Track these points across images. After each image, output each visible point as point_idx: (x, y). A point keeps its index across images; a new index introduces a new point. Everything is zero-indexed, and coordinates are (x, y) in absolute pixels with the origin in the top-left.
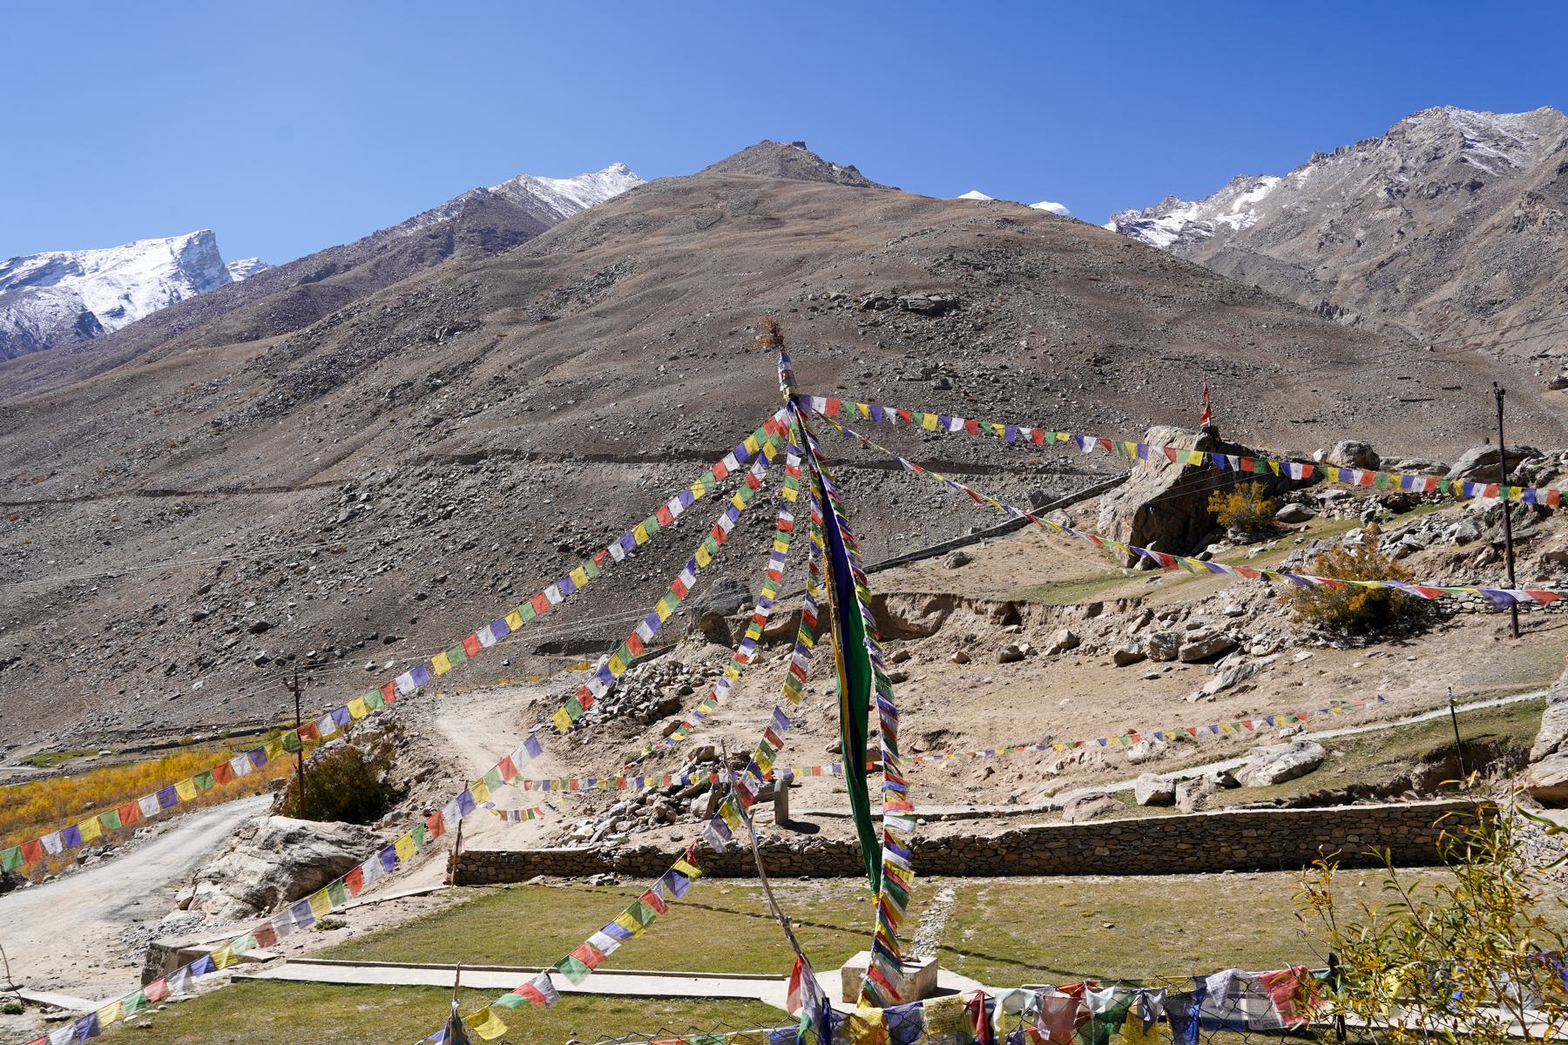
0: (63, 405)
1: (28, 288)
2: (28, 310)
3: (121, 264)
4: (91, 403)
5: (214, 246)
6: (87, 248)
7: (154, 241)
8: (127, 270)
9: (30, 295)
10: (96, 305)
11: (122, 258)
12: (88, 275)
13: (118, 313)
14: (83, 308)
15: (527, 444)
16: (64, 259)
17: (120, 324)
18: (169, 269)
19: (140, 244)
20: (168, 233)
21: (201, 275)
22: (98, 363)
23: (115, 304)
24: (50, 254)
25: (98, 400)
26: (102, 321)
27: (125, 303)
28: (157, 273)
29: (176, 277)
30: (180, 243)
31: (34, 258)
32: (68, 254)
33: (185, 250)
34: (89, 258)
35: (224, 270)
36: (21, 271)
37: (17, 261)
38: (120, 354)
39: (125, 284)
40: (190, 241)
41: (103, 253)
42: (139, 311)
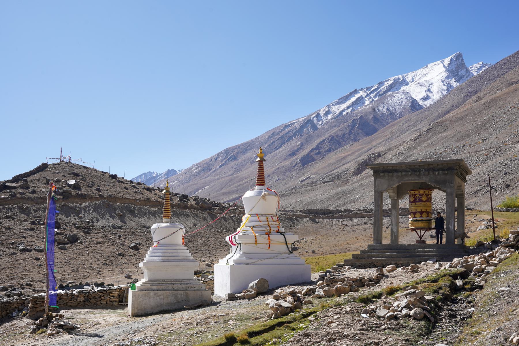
0: (462, 118)
1: (389, 93)
2: (391, 102)
3: (422, 77)
4: (476, 114)
5: (462, 60)
6: (407, 72)
7: (435, 63)
8: (426, 78)
9: (391, 96)
10: (416, 96)
11: (422, 74)
12: (410, 84)
13: (427, 98)
14: (412, 98)
15: (160, 289)
16: (399, 79)
17: (428, 103)
18: (445, 74)
19: (430, 65)
20: (441, 59)
21: (457, 75)
22: (436, 115)
23: (424, 94)
24: (393, 78)
25: (478, 113)
26: (420, 103)
27: (428, 93)
28: (440, 77)
29: (447, 77)
30: (447, 61)
31: (388, 81)
32: (400, 76)
33: (449, 64)
34: (409, 77)
35: (467, 71)
36: (383, 88)
37: (381, 84)
38: (444, 109)
39: (427, 85)
40: (451, 60)
41: (414, 73)
42: (436, 96)
